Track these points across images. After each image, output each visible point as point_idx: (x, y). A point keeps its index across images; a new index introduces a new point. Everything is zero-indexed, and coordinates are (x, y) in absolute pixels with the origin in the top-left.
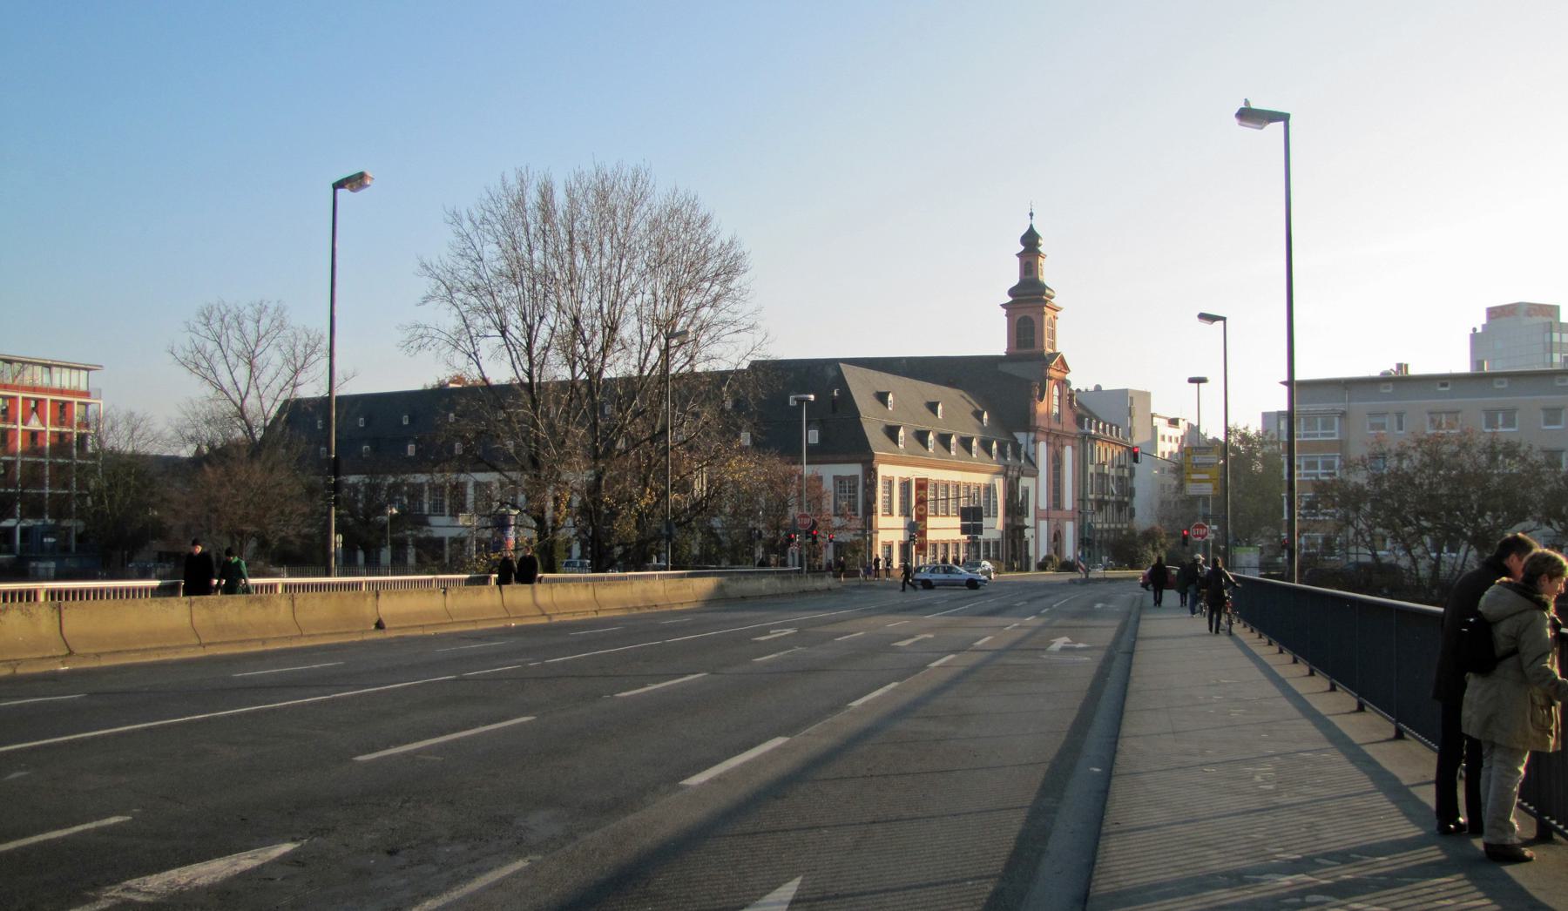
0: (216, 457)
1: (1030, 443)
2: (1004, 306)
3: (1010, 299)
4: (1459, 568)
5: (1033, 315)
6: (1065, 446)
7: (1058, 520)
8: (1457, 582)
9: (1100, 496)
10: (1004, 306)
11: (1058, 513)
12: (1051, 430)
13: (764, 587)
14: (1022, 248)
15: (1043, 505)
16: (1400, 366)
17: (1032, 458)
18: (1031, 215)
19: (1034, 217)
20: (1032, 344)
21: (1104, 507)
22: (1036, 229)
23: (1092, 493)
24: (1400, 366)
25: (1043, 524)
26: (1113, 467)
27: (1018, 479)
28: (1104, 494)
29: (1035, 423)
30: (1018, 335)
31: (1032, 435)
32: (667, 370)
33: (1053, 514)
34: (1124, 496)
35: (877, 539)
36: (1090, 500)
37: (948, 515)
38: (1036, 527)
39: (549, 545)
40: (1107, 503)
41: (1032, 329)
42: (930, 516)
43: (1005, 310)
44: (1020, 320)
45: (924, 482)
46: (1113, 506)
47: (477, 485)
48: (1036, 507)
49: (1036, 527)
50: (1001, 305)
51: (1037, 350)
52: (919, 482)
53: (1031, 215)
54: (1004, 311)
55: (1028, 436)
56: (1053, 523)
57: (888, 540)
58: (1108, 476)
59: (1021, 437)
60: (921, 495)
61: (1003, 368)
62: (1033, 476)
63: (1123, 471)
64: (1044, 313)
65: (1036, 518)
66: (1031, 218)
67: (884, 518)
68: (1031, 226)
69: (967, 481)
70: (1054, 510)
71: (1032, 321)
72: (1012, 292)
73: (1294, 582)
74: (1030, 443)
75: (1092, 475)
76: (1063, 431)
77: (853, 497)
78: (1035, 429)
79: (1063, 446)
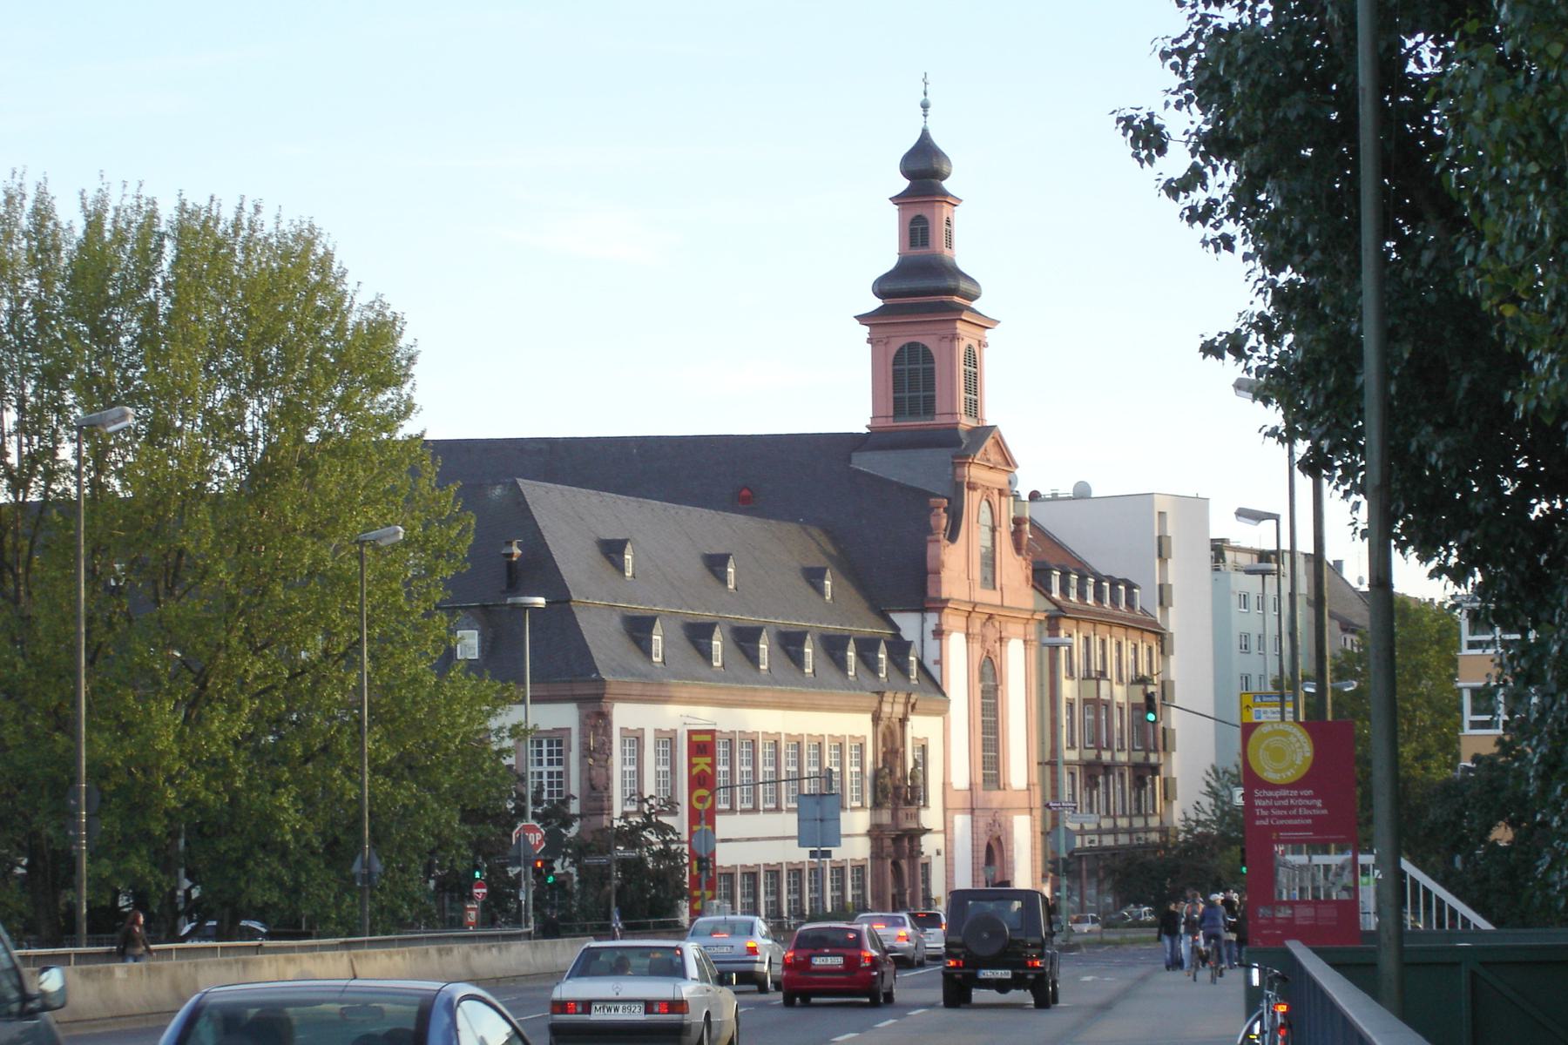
1: (929, 636)
2: (863, 319)
5: (930, 342)
10: (863, 319)
14: (904, 184)
15: (960, 780)
17: (934, 670)
18: (925, 106)
19: (930, 111)
20: (929, 407)
21: (1101, 779)
22: (939, 140)
23: (1072, 747)
25: (961, 822)
27: (903, 721)
29: (939, 591)
30: (898, 385)
31: (932, 619)
36: (1069, 763)
40: (1108, 769)
42: (723, 812)
43: (867, 329)
45: (708, 738)
51: (945, 420)
52: (696, 738)
53: (925, 106)
55: (923, 621)
60: (702, 766)
61: (863, 462)
62: (938, 714)
64: (954, 337)
65: (945, 809)
66: (925, 116)
68: (925, 135)
71: (928, 356)
74: (929, 636)
75: (1071, 704)
77: (560, 774)
78: (939, 605)
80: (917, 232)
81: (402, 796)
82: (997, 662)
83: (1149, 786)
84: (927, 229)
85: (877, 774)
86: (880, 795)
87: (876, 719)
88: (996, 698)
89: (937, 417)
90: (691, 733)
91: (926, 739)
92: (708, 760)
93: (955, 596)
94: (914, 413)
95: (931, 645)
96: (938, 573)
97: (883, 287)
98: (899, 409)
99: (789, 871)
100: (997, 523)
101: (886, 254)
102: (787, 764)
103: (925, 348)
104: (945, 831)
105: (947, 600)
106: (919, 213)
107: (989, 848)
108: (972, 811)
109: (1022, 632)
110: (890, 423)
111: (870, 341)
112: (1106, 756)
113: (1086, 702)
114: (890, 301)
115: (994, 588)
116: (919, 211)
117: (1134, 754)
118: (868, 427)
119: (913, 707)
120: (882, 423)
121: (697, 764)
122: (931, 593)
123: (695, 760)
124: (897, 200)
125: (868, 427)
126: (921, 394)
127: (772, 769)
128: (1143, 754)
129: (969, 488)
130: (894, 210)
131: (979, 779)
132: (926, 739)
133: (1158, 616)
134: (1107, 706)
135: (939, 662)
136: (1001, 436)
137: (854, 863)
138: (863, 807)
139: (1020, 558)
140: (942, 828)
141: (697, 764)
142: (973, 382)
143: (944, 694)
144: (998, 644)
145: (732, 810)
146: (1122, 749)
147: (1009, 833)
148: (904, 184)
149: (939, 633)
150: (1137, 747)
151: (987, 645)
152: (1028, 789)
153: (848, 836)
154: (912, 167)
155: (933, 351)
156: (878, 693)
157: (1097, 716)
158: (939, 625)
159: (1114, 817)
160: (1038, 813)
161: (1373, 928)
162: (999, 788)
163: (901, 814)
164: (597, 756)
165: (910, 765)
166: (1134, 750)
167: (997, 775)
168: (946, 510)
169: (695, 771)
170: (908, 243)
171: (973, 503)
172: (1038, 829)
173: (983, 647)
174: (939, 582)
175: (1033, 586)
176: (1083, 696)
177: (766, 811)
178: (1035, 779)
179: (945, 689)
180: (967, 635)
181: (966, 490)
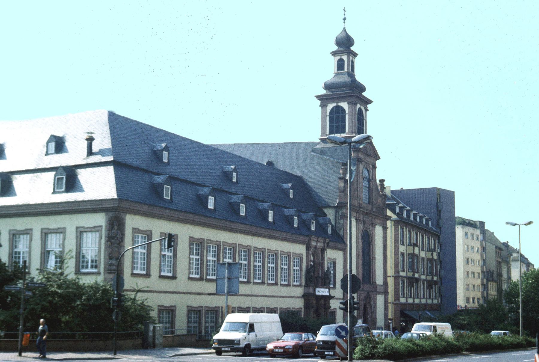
2: (319, 97)
7: (368, 293)
10: (319, 97)
16: (401, 188)
21: (433, 286)
23: (403, 271)
24: (401, 188)
26: (423, 250)
27: (323, 250)
28: (414, 272)
32: (136, 293)
34: (433, 276)
39: (332, 54)
40: (417, 280)
43: (320, 102)
45: (277, 252)
46: (423, 284)
47: (63, 178)
50: (315, 96)
54: (319, 102)
58: (417, 256)
63: (432, 254)
67: (101, 225)
69: (285, 250)
79: (373, 225)
83: (434, 289)
85: (308, 271)
87: (308, 248)
91: (335, 259)
102: (282, 264)
112: (417, 275)
113: (409, 254)
117: (428, 277)
119: (328, 244)
120: (457, 219)
126: (335, 124)
127: (298, 268)
132: (335, 259)
134: (435, 261)
137: (207, 309)
138: (300, 286)
144: (371, 227)
146: (424, 274)
153: (298, 297)
157: (432, 264)
159: (407, 298)
166: (428, 275)
176: (427, 257)
177: (294, 286)
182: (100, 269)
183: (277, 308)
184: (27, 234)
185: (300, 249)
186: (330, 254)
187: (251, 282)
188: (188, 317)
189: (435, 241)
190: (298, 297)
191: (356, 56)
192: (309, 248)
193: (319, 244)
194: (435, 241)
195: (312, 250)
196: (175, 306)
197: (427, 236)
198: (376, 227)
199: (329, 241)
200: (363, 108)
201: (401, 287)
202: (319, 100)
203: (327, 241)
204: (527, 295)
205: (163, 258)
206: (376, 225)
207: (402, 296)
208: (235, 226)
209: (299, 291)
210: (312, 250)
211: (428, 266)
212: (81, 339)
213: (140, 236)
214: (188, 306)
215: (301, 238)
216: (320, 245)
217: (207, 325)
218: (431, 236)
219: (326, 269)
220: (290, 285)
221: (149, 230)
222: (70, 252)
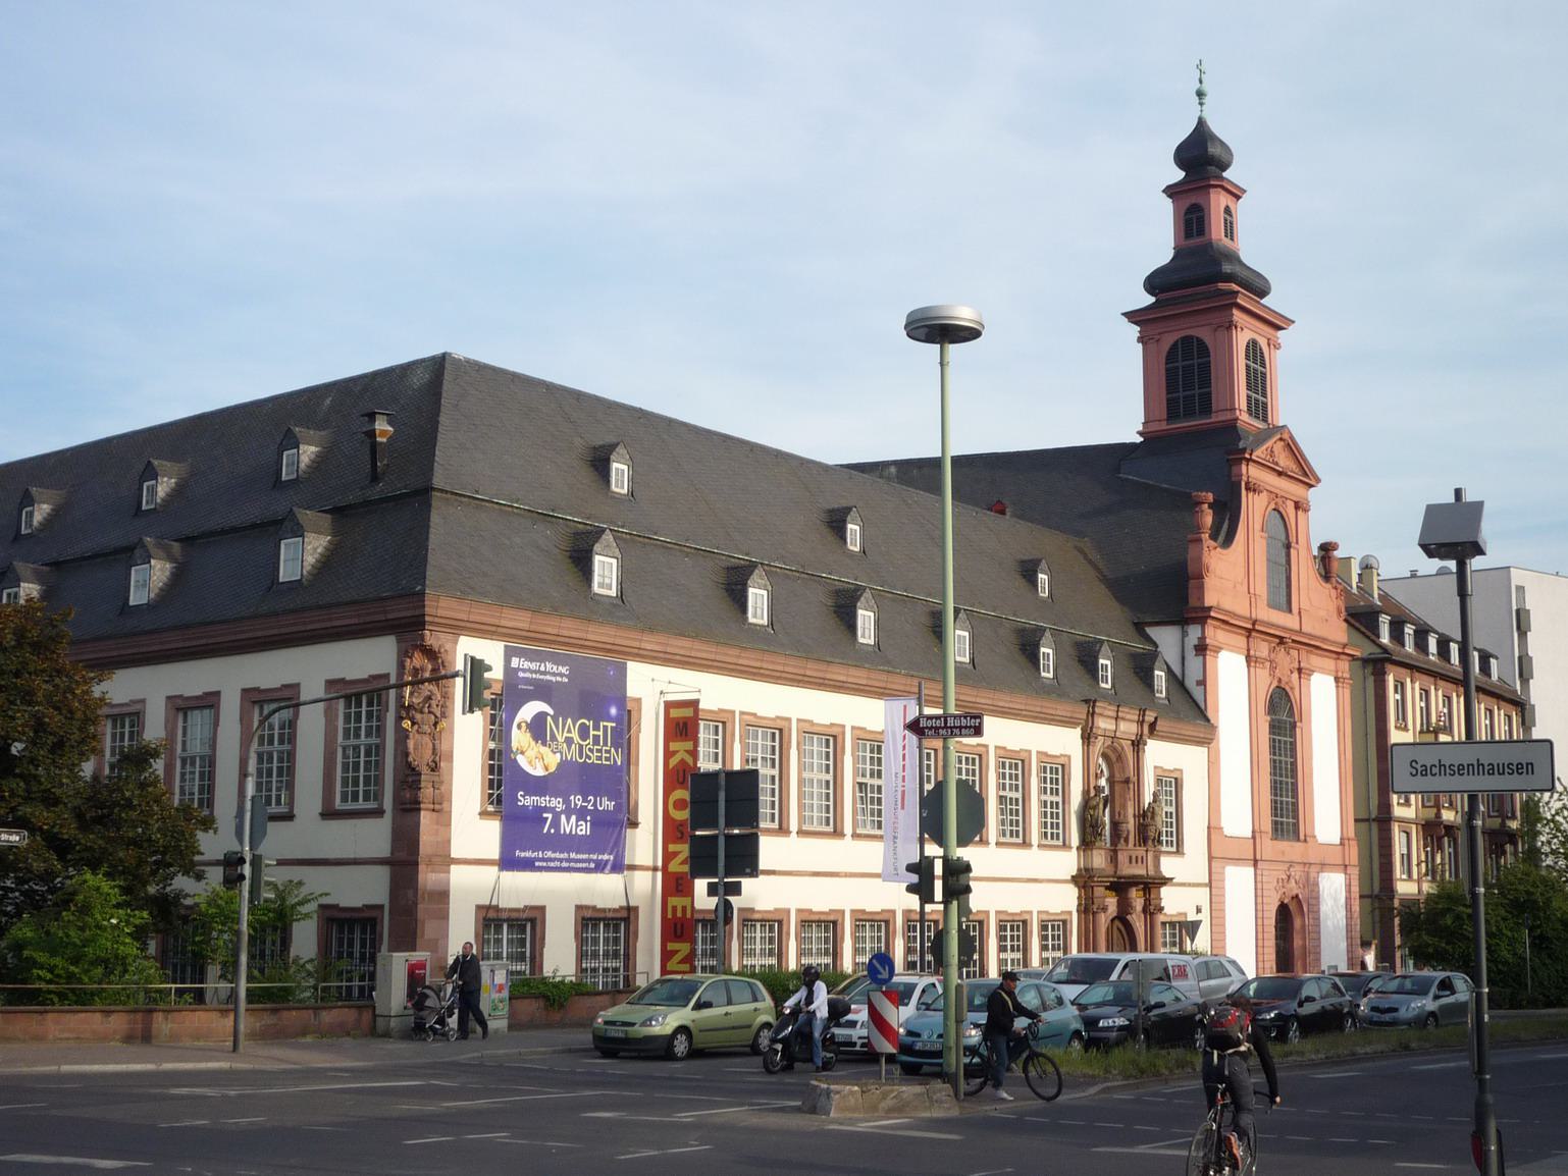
0: (1128, 899)
1: (1190, 653)
2: (1133, 316)
3: (1151, 300)
4: (1253, 664)
5: (1208, 339)
6: (1311, 672)
8: (268, 1006)
9: (1431, 813)
10: (1133, 316)
11: (1290, 849)
12: (1254, 623)
13: (265, 1017)
14: (1179, 175)
17: (1197, 692)
18: (1200, 94)
19: (1206, 100)
20: (1206, 407)
22: (1216, 127)
25: (1239, 882)
27: (1138, 744)
29: (1201, 598)
30: (1171, 386)
31: (1194, 632)
33: (1269, 847)
35: (443, 896)
37: (837, 833)
38: (1213, 884)
41: (1205, 370)
42: (769, 832)
44: (1175, 345)
45: (688, 712)
48: (1213, 829)
49: (1210, 885)
50: (1124, 314)
51: (1222, 417)
53: (1200, 94)
54: (1134, 331)
55: (1184, 634)
56: (1273, 874)
57: (675, 904)
59: (1166, 638)
62: (1199, 742)
64: (1230, 326)
65: (1211, 858)
66: (1201, 104)
68: (1201, 123)
70: (1275, 838)
71: (1203, 350)
72: (1153, 283)
73: (176, 988)
74: (1190, 653)
76: (1300, 631)
78: (1202, 615)
80: (1192, 221)
81: (43, 780)
82: (1295, 696)
84: (1203, 217)
86: (1089, 830)
87: (1087, 737)
88: (1293, 735)
89: (1213, 415)
90: (669, 705)
92: (689, 745)
93: (1227, 604)
94: (1190, 413)
95: (1194, 662)
96: (1200, 577)
97: (1155, 283)
98: (1172, 414)
99: (1002, 928)
100: (1293, 539)
101: (1158, 244)
103: (1200, 342)
104: (1210, 885)
105: (1210, 609)
106: (1193, 201)
107: (1284, 913)
108: (1255, 862)
109: (1333, 668)
110: (1164, 426)
111: (1140, 340)
114: (1163, 296)
115: (1290, 611)
116: (1193, 199)
118: (1140, 433)
119: (1152, 726)
120: (1155, 427)
121: (674, 753)
122: (1193, 602)
123: (673, 746)
124: (1172, 191)
125: (1140, 433)
128: (1499, 820)
129: (1248, 489)
130: (1167, 206)
131: (1267, 825)
133: (1518, 688)
135: (1202, 683)
136: (1292, 437)
139: (1328, 586)
140: (1207, 881)
141: (674, 753)
142: (1258, 381)
143: (1208, 720)
144: (1295, 675)
145: (783, 830)
147: (1315, 898)
148: (1179, 175)
149: (1202, 649)
150: (1492, 814)
151: (1278, 673)
152: (1342, 844)
154: (1422, 543)
155: (1210, 346)
156: (1087, 701)
158: (1203, 638)
160: (1355, 872)
161: (513, 659)
162: (1298, 840)
163: (1122, 857)
164: (418, 716)
165: (1148, 799)
166: (1489, 816)
167: (1296, 825)
168: (1211, 506)
169: (673, 762)
170: (1182, 234)
171: (1254, 508)
172: (1355, 889)
173: (1272, 673)
174: (1201, 588)
175: (1346, 620)
178: (1351, 833)
179: (1210, 714)
180: (1248, 658)
181: (1244, 492)
182: (382, 802)
183: (1031, 913)
184: (211, 707)
185: (1064, 741)
186: (1159, 755)
187: (1070, 848)
188: (581, 941)
189: (1510, 718)
190: (1065, 881)
191: (1238, 197)
192: (1088, 739)
193: (1123, 726)
194: (1510, 718)
195: (1099, 745)
196: (542, 909)
197: (1502, 711)
198: (1313, 678)
199: (1156, 718)
200: (1263, 342)
201: (1450, 854)
202: (1136, 323)
203: (1150, 717)
204: (21, 703)
205: (861, 792)
206: (1221, 648)
207: (1404, 877)
208: (838, 673)
209: (1068, 862)
210: (1099, 745)
211: (982, 709)
212: (1470, 950)
213: (815, 740)
214: (579, 908)
215: (1063, 709)
216: (1128, 728)
217: (1045, 955)
218: (1435, 685)
219: (1148, 799)
220: (1070, 848)
221: (1026, 751)
222: (681, 780)
